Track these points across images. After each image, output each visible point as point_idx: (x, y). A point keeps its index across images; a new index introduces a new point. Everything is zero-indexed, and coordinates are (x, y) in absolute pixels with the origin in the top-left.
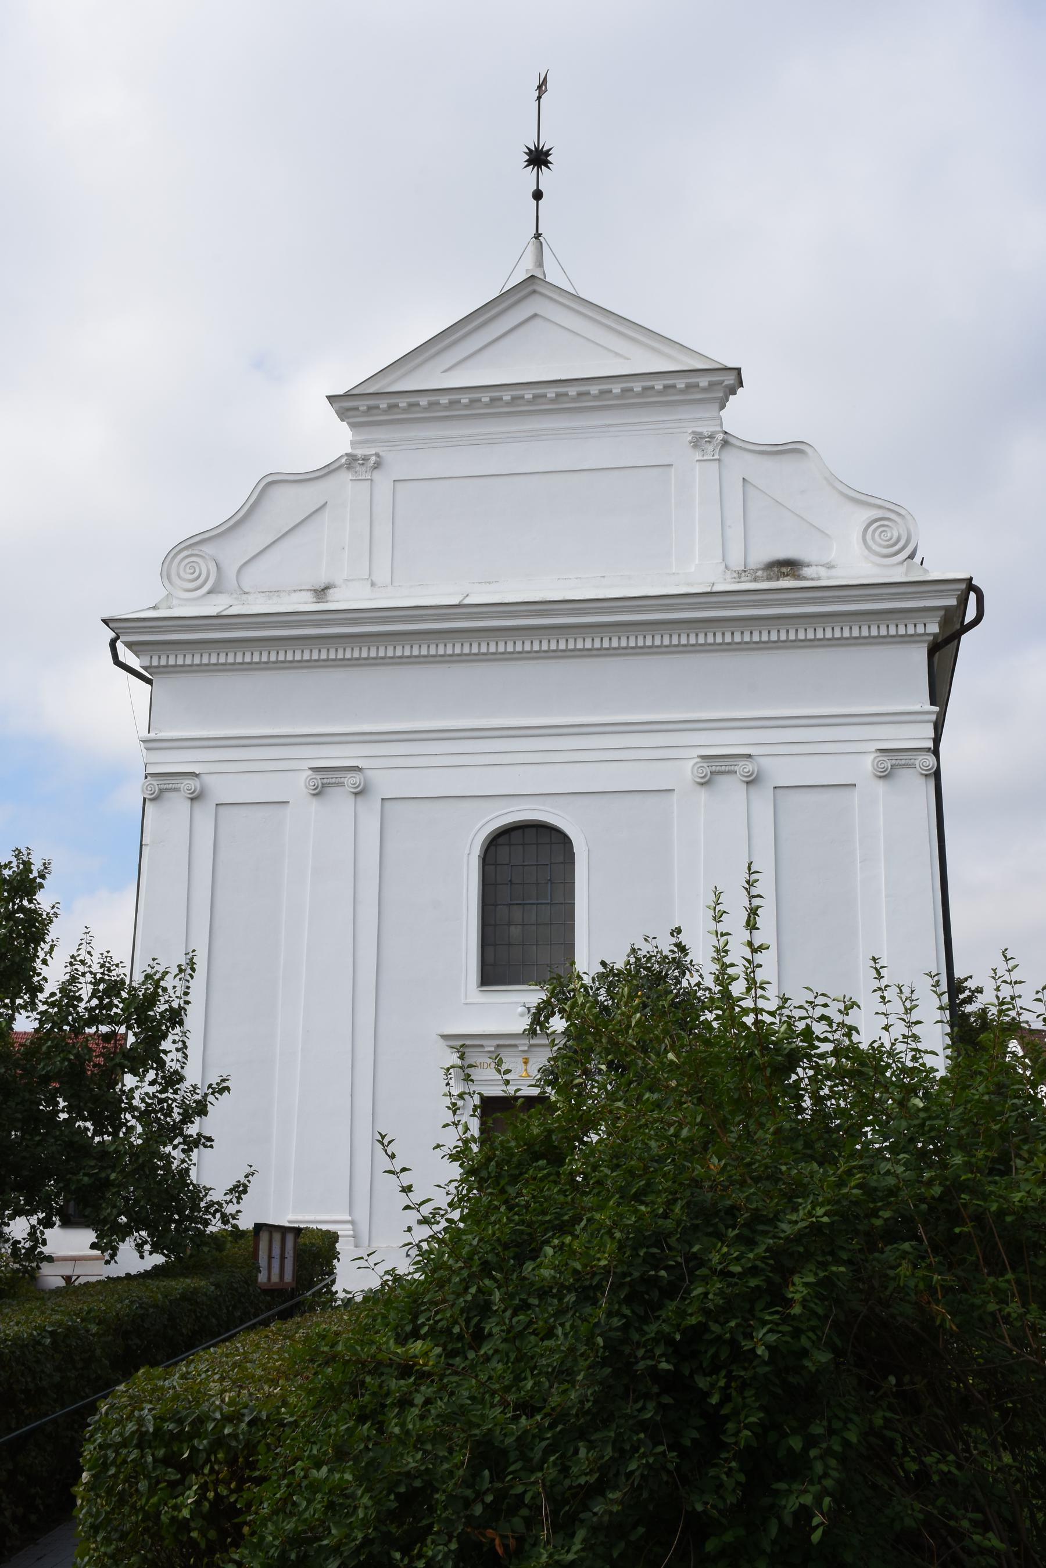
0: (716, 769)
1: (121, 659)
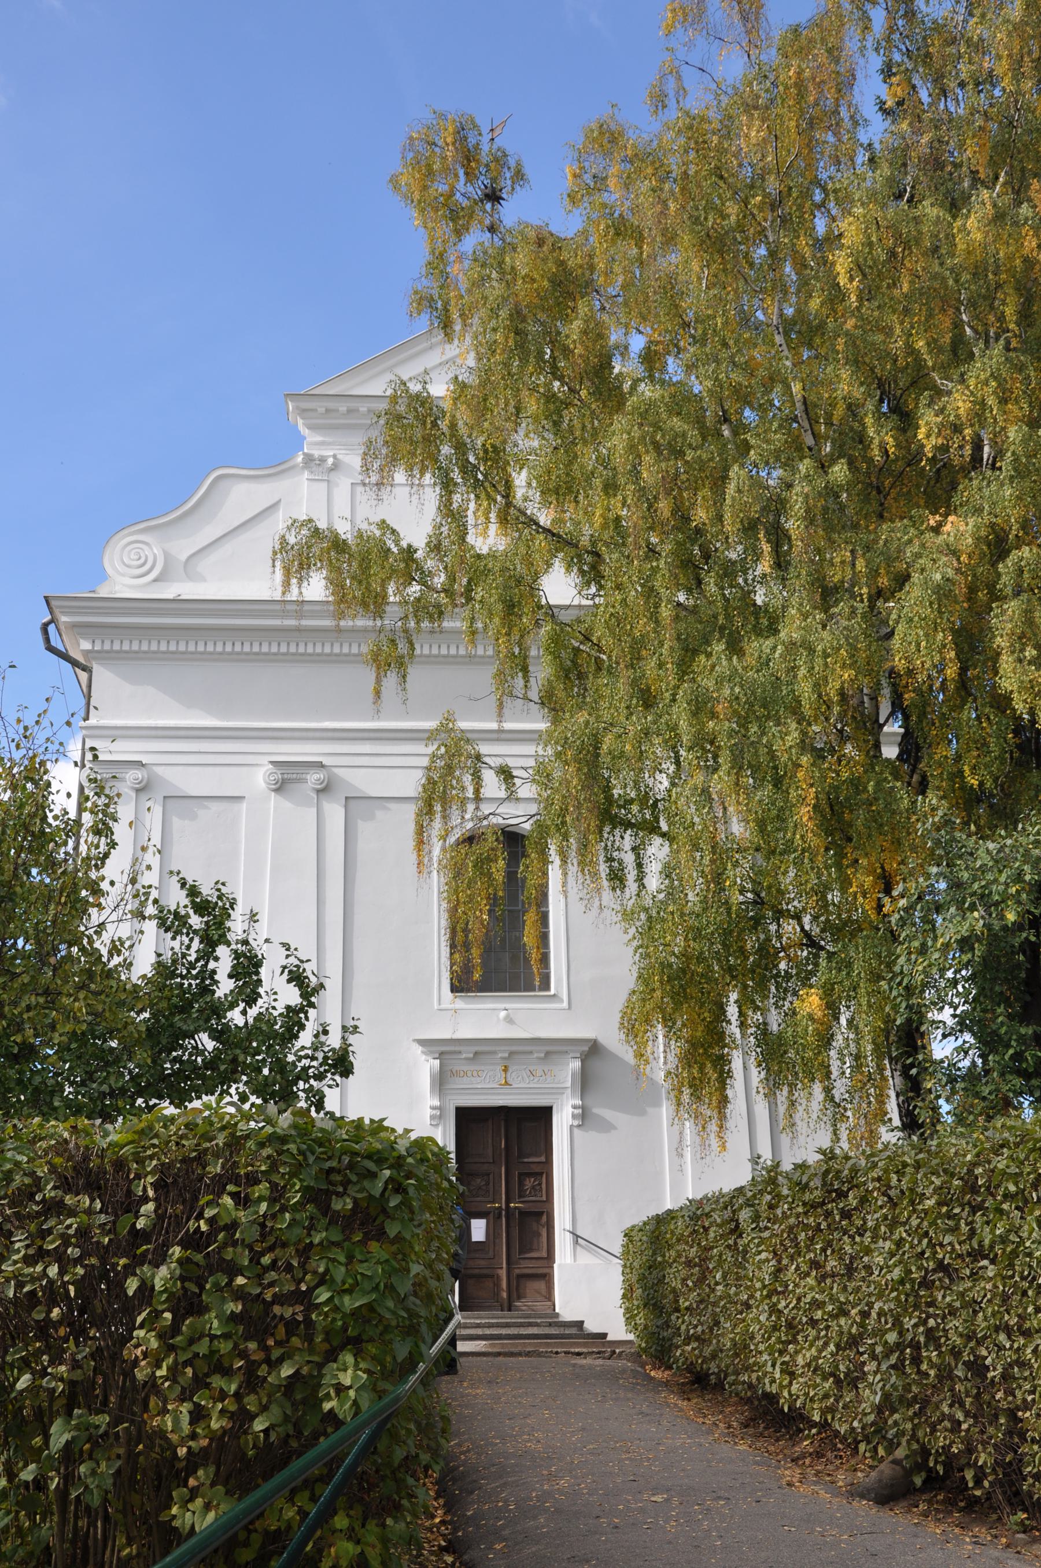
0: (287, 779)
1: (53, 643)
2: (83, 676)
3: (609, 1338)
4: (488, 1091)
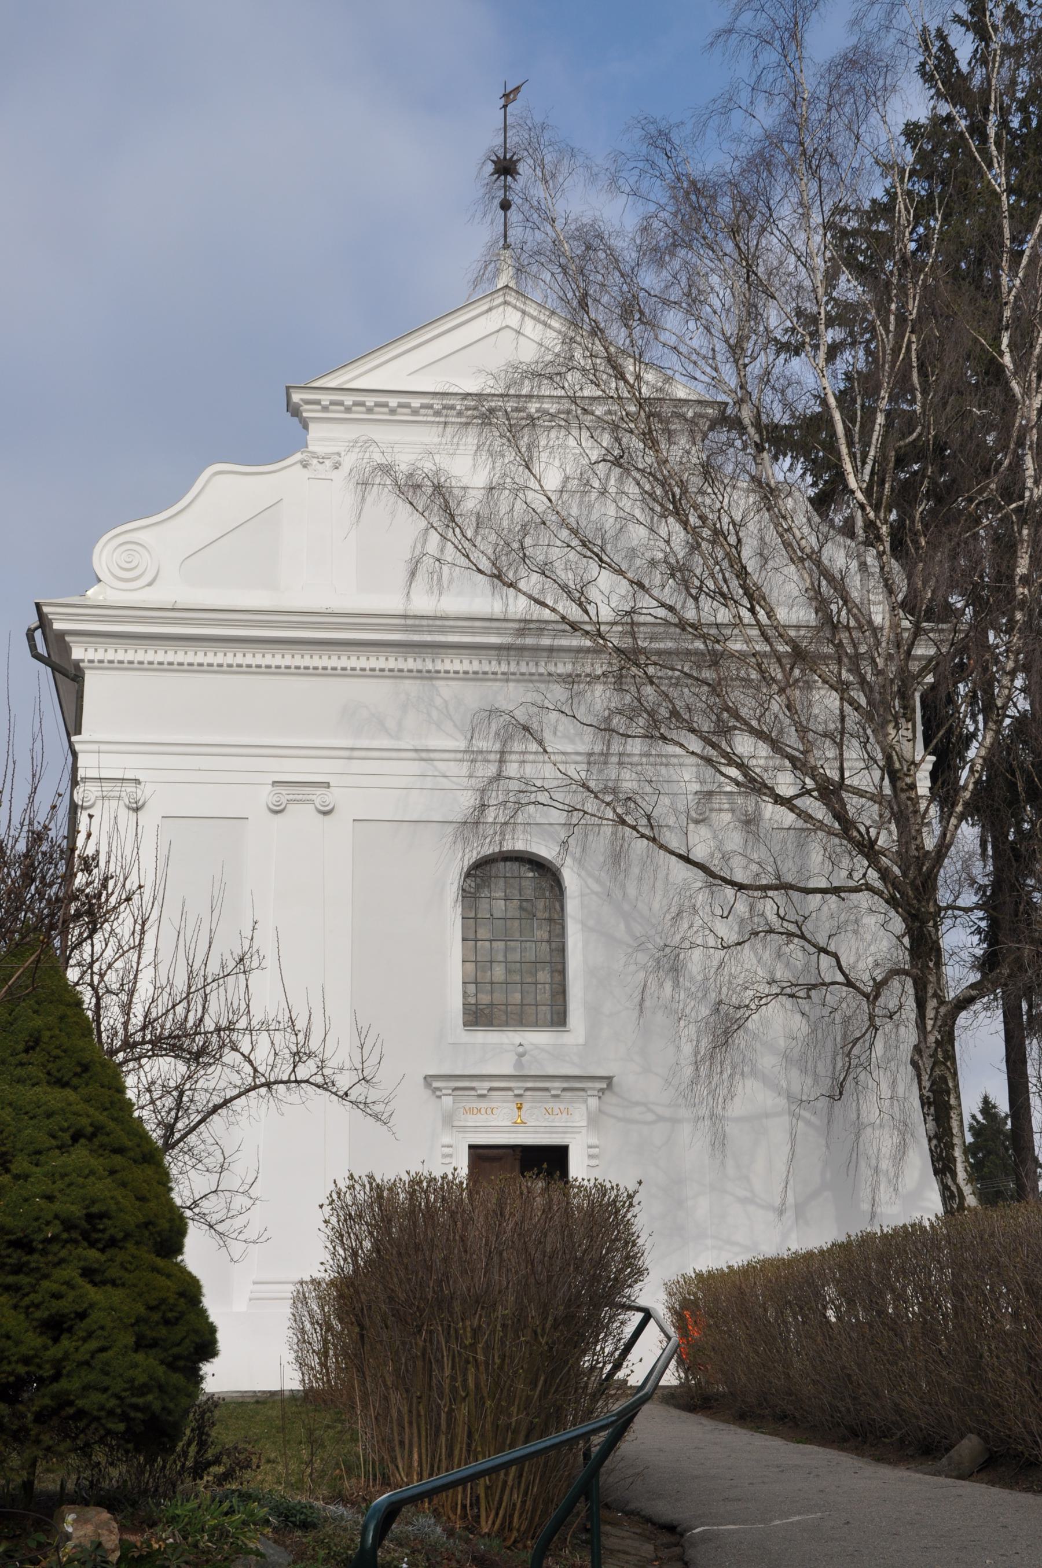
4: (506, 1126)
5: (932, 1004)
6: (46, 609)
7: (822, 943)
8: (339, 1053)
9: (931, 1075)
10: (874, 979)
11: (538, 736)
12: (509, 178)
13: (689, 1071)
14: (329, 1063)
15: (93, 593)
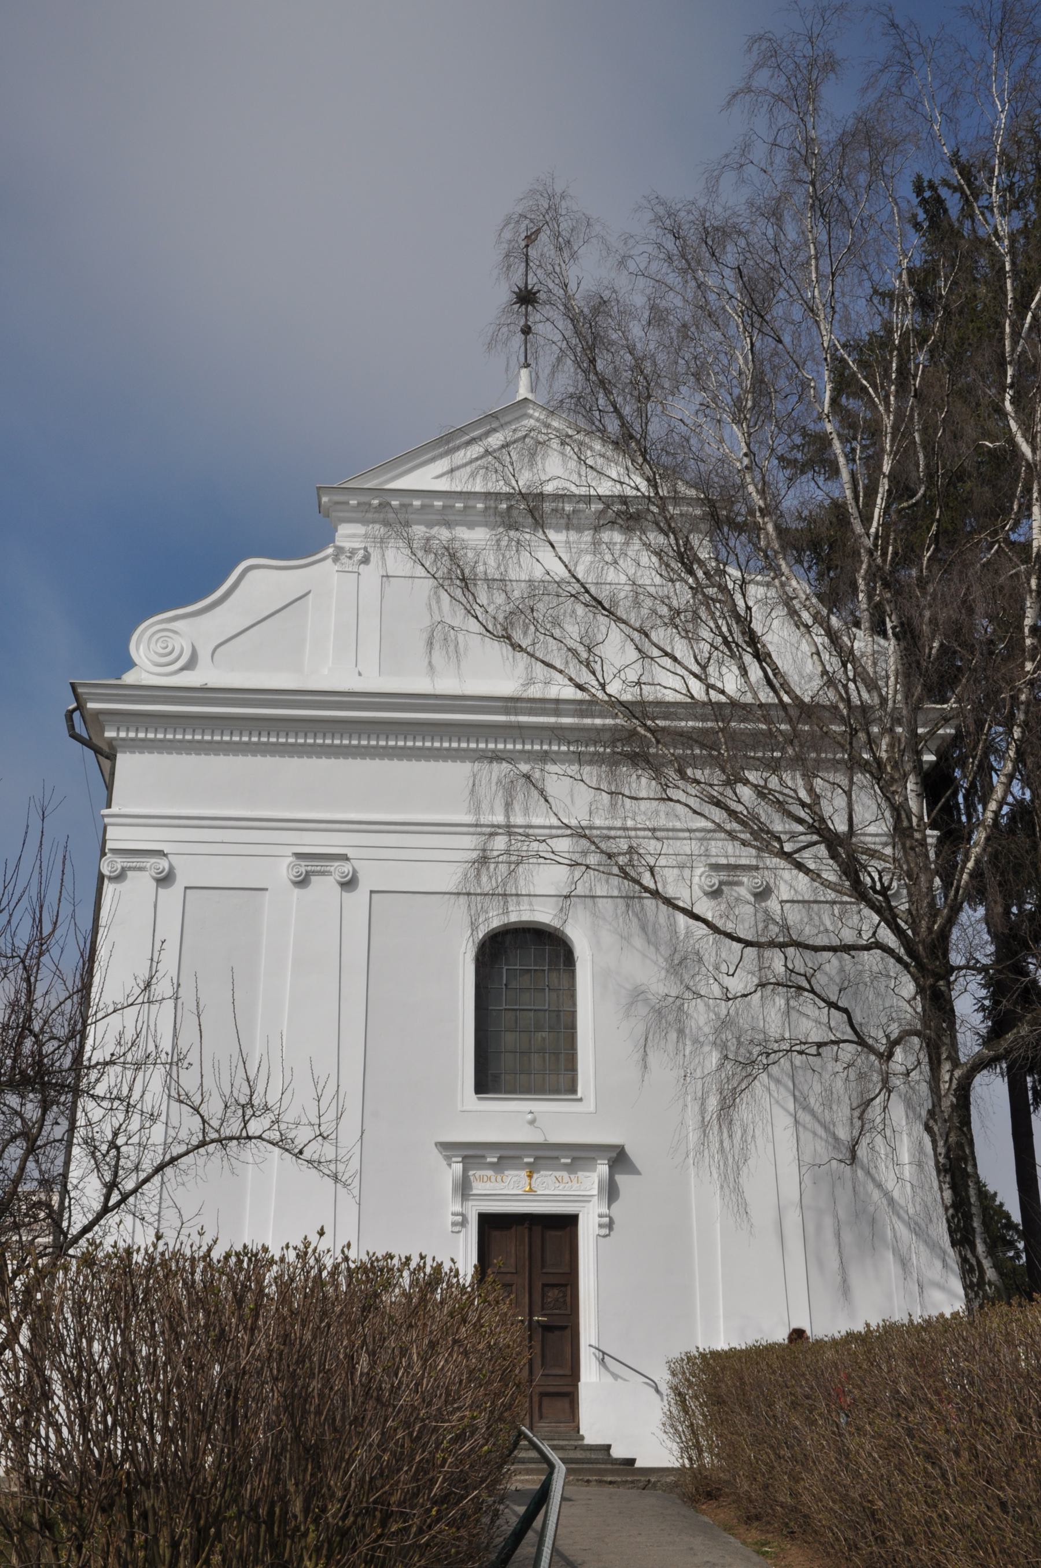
0: (309, 869)
1: (77, 730)
2: (106, 763)
3: (637, 1465)
4: (512, 1192)
5: (946, 1066)
6: (80, 690)
7: (833, 998)
8: (298, 1109)
9: (946, 1141)
10: (887, 1036)
11: (540, 785)
12: (530, 308)
13: (693, 1137)
14: (284, 1118)
15: (130, 678)
